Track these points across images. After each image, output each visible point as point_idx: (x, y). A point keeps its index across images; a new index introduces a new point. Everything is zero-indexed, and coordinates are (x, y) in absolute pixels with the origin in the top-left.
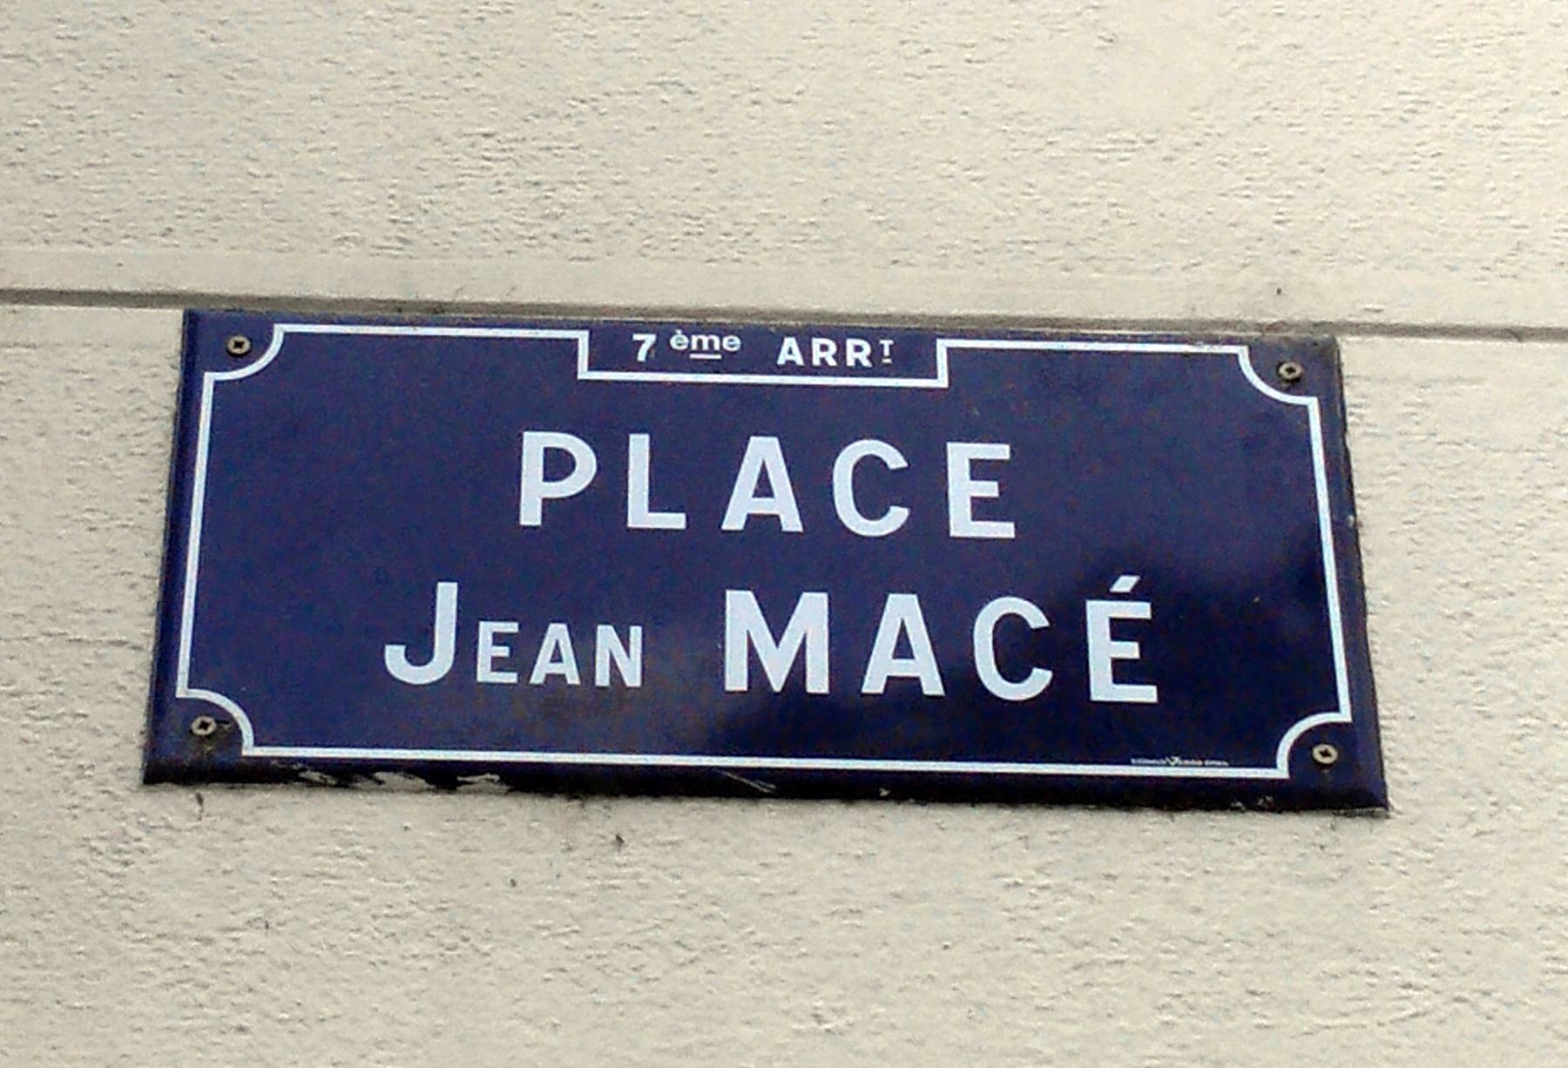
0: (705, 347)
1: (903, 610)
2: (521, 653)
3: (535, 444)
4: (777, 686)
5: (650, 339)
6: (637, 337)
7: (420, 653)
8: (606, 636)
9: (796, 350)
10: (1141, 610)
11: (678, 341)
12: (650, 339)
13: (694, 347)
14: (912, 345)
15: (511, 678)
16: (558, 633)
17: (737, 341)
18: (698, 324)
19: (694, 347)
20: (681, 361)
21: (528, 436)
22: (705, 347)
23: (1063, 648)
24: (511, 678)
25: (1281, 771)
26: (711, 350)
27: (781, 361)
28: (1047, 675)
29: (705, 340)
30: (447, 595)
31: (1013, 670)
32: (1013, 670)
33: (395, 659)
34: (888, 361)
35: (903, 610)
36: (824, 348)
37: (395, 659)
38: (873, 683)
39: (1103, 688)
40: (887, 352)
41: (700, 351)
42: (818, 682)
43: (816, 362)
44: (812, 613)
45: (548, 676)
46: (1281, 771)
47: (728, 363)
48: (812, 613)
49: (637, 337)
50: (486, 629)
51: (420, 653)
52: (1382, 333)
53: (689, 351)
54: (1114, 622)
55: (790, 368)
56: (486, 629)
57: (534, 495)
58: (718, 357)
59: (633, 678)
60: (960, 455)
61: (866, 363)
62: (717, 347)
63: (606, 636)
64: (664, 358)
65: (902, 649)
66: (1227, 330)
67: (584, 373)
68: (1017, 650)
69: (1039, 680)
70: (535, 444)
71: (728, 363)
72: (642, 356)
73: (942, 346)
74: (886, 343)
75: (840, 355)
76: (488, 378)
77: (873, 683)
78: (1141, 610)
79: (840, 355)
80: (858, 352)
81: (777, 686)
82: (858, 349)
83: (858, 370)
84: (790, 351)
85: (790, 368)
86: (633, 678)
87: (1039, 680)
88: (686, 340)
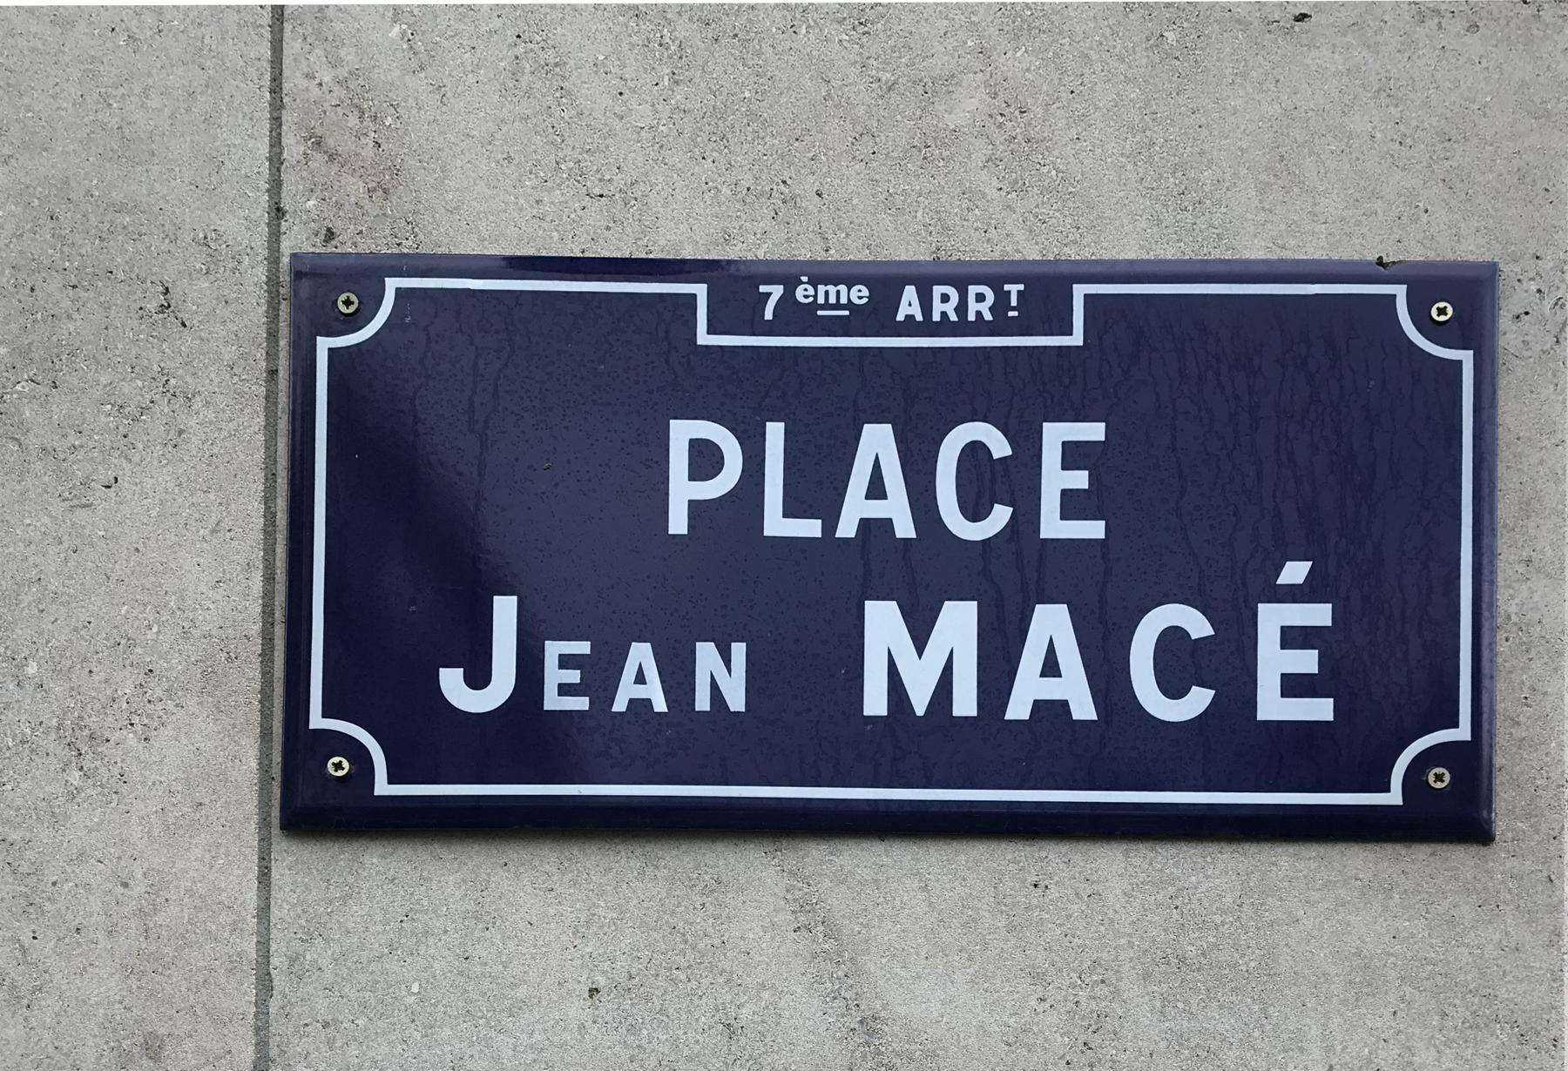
0: (832, 300)
1: (1051, 623)
2: (600, 674)
3: (682, 432)
4: (920, 710)
5: (777, 291)
6: (763, 289)
7: (478, 678)
8: (706, 653)
9: (916, 302)
10: (1319, 615)
11: (802, 293)
12: (777, 291)
13: (821, 300)
14: (1045, 293)
15: (581, 703)
16: (641, 654)
17: (865, 292)
18: (823, 274)
19: (821, 300)
20: (796, 317)
21: (1048, 427)
22: (832, 300)
23: (1224, 662)
24: (581, 703)
25: (1394, 797)
26: (838, 306)
27: (900, 317)
28: (1209, 694)
29: (832, 289)
30: (505, 610)
31: (1173, 687)
32: (1173, 687)
33: (451, 681)
34: (1015, 314)
35: (1051, 623)
36: (945, 298)
37: (451, 681)
38: (1018, 709)
39: (1272, 706)
40: (1014, 303)
41: (827, 306)
42: (965, 703)
43: (936, 317)
44: (958, 623)
45: (631, 701)
46: (1394, 797)
47: (858, 321)
48: (958, 623)
49: (763, 289)
50: (554, 649)
51: (478, 678)
52: (278, 242)
53: (814, 306)
54: (1285, 631)
55: (910, 327)
56: (554, 649)
57: (683, 491)
58: (847, 313)
59: (736, 700)
60: (1055, 434)
61: (988, 316)
62: (844, 300)
63: (706, 653)
64: (796, 317)
65: (1053, 668)
66: (1382, 270)
67: (704, 338)
68: (1179, 663)
69: (1198, 700)
70: (682, 432)
71: (858, 321)
72: (769, 315)
73: (1080, 291)
74: (1014, 289)
75: (962, 308)
76: (611, 342)
77: (1018, 709)
78: (1319, 615)
79: (962, 308)
80: (981, 306)
81: (920, 710)
82: (980, 298)
83: (980, 327)
84: (909, 304)
85: (910, 327)
86: (736, 700)
87: (1198, 700)
88: (811, 291)
